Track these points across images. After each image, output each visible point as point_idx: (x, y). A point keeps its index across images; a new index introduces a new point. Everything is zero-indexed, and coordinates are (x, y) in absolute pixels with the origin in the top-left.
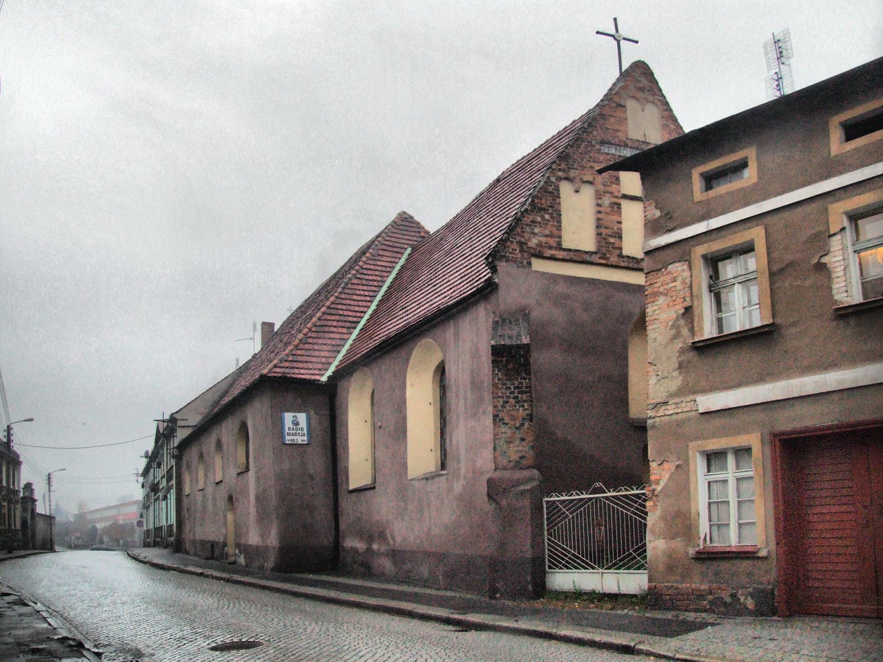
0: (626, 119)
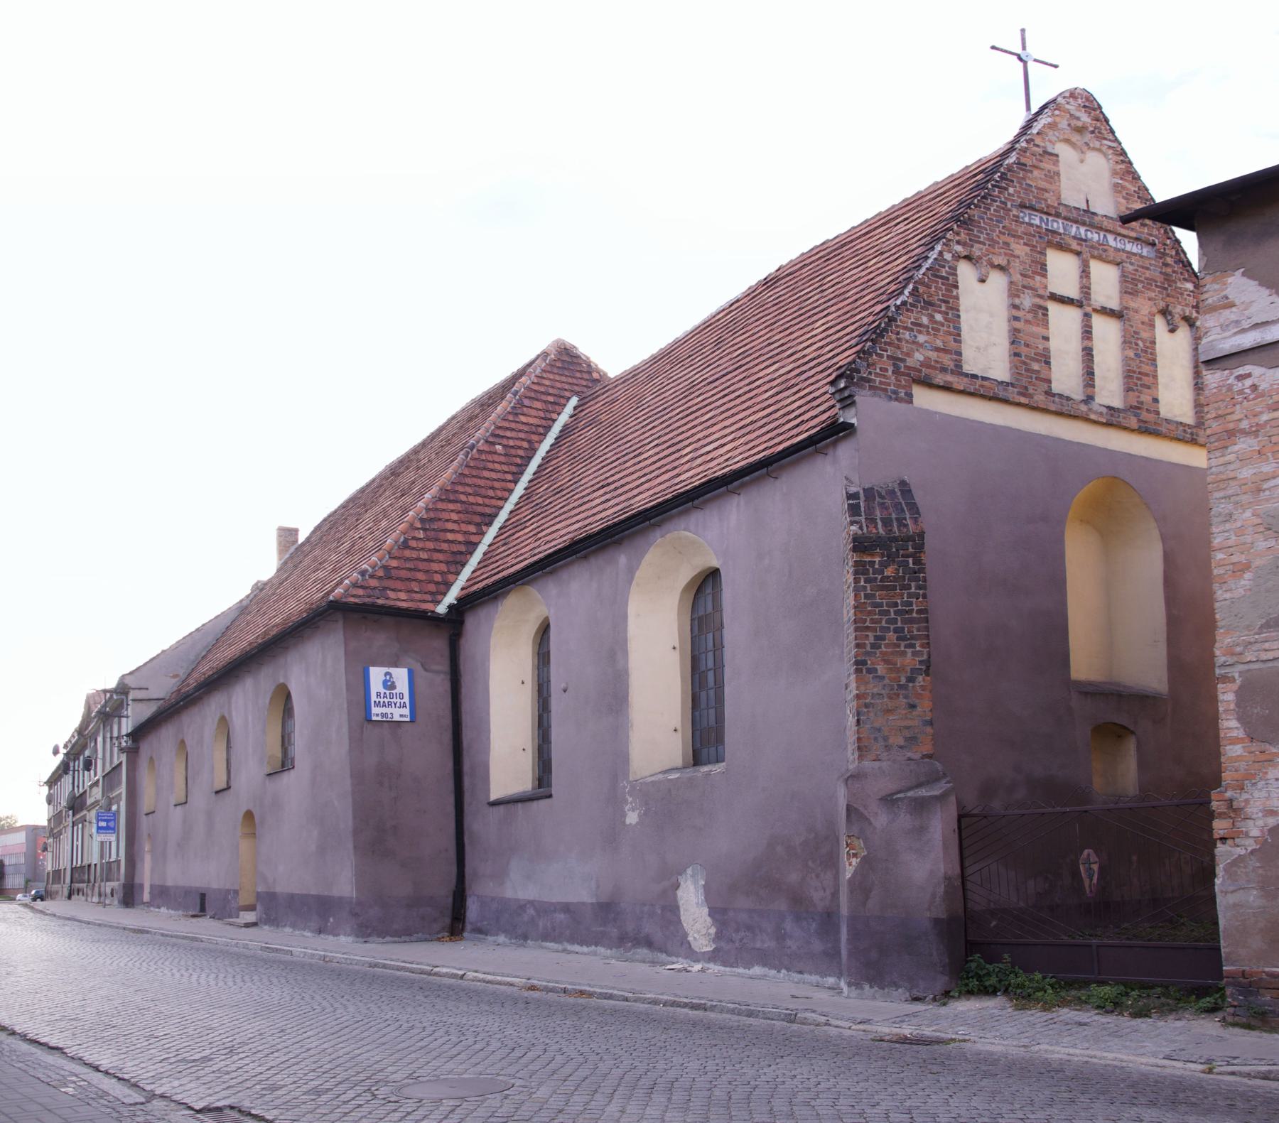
0: (1058, 174)
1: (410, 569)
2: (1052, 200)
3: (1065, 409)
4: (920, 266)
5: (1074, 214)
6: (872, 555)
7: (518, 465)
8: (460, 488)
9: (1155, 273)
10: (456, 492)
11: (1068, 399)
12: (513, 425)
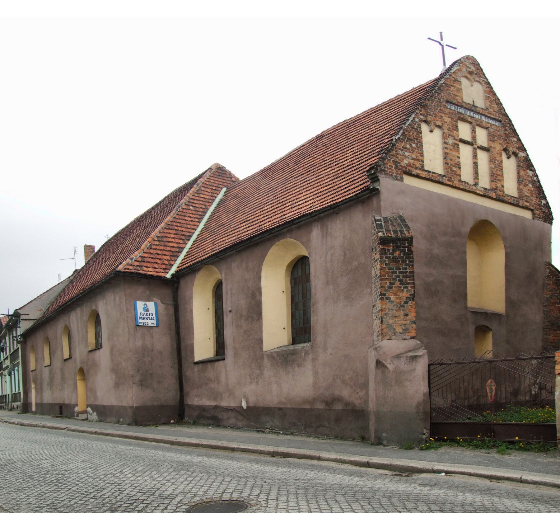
0: (461, 89)
1: (153, 258)
2: (459, 100)
3: (467, 188)
4: (405, 123)
5: (468, 106)
6: (388, 246)
7: (200, 215)
8: (175, 224)
9: (502, 133)
10: (173, 225)
11: (468, 183)
12: (197, 198)
